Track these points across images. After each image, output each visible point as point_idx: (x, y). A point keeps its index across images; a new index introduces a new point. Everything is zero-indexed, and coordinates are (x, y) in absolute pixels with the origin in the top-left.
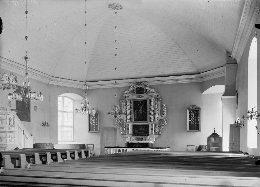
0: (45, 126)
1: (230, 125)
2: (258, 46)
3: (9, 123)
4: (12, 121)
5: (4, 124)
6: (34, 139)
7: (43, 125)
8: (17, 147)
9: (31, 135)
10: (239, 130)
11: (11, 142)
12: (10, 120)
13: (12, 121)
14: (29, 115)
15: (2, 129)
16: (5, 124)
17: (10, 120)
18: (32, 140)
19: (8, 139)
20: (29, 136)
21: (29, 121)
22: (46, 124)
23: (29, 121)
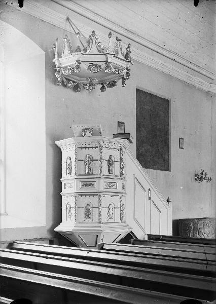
0: (200, 180)
1: (167, 102)
2: (27, 261)
3: (109, 170)
4: (117, 165)
5: (95, 173)
6: (174, 212)
7: (196, 180)
8: (131, 232)
9: (168, 201)
10: (42, 47)
11: (112, 220)
12: (110, 162)
13: (117, 165)
14: (167, 157)
15: (92, 185)
16: (96, 171)
17: (110, 162)
18: (170, 210)
19: (104, 212)
20: (161, 204)
21: (167, 168)
22: (204, 176)
23: (167, 168)
